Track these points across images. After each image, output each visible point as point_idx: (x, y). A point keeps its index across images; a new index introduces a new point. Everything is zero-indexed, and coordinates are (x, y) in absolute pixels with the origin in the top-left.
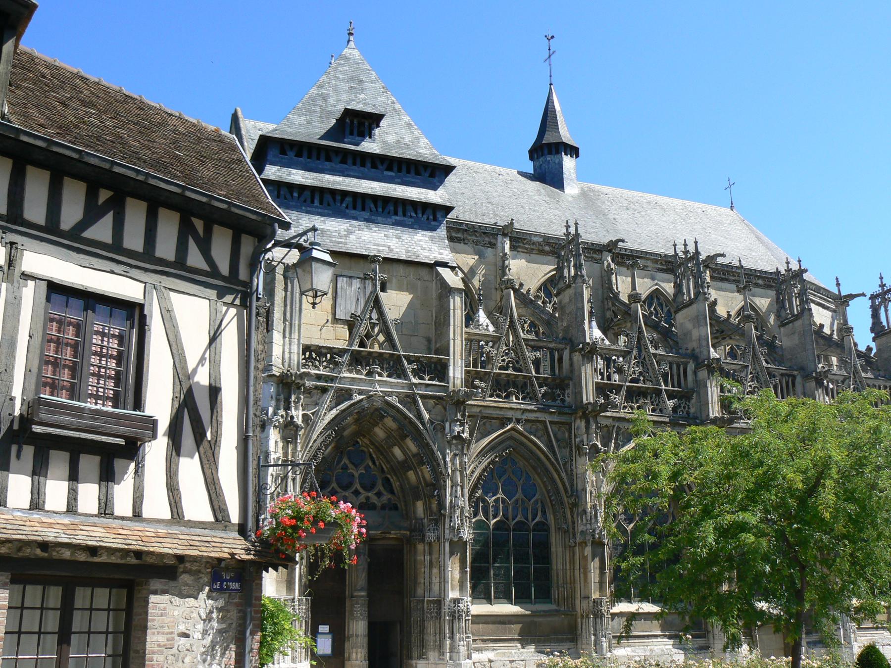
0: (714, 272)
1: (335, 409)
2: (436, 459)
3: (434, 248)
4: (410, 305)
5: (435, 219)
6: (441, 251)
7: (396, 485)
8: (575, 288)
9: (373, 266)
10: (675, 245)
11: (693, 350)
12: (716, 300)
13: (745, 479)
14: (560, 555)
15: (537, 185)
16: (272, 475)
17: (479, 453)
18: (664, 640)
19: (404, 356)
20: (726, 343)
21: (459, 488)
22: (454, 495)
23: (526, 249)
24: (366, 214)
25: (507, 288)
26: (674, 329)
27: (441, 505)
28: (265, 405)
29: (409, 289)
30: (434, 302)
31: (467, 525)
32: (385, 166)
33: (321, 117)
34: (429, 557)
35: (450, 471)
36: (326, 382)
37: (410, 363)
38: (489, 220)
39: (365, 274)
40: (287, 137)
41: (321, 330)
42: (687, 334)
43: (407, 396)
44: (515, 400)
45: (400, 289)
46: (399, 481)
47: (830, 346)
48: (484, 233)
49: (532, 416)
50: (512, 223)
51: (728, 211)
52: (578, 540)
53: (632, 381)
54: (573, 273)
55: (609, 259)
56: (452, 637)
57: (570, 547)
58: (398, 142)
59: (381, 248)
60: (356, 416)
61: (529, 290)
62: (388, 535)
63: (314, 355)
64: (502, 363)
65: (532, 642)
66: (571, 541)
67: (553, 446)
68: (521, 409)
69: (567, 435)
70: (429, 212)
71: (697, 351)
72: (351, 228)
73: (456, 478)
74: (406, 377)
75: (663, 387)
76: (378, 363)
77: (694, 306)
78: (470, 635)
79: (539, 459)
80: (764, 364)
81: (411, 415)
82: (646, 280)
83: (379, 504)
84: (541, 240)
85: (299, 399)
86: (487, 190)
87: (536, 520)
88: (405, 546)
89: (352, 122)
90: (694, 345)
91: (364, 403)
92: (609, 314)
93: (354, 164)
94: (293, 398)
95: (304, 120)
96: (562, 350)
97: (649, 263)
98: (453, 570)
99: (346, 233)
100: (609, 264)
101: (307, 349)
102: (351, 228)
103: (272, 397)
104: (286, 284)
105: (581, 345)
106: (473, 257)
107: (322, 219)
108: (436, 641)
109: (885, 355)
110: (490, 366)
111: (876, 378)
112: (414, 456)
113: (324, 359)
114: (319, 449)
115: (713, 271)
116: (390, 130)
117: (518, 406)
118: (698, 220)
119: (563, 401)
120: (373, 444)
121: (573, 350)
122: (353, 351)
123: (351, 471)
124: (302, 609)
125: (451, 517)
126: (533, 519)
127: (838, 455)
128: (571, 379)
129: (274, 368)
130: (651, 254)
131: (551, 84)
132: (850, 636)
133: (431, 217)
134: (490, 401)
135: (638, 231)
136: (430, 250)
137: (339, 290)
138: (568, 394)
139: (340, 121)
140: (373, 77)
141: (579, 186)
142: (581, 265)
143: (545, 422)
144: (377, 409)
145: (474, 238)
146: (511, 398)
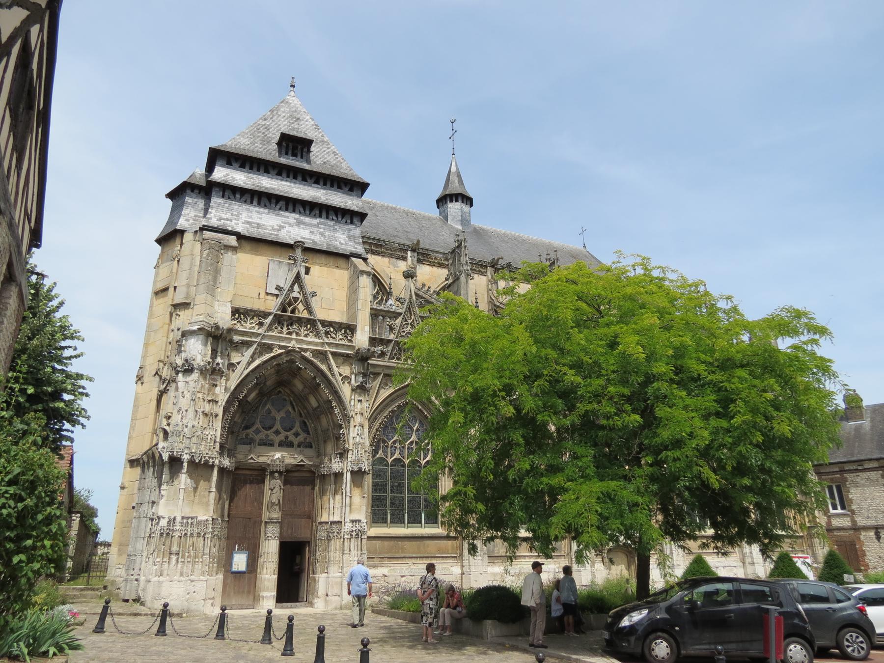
23: (430, 262)
50: (418, 241)
63: (242, 316)
126: (424, 459)
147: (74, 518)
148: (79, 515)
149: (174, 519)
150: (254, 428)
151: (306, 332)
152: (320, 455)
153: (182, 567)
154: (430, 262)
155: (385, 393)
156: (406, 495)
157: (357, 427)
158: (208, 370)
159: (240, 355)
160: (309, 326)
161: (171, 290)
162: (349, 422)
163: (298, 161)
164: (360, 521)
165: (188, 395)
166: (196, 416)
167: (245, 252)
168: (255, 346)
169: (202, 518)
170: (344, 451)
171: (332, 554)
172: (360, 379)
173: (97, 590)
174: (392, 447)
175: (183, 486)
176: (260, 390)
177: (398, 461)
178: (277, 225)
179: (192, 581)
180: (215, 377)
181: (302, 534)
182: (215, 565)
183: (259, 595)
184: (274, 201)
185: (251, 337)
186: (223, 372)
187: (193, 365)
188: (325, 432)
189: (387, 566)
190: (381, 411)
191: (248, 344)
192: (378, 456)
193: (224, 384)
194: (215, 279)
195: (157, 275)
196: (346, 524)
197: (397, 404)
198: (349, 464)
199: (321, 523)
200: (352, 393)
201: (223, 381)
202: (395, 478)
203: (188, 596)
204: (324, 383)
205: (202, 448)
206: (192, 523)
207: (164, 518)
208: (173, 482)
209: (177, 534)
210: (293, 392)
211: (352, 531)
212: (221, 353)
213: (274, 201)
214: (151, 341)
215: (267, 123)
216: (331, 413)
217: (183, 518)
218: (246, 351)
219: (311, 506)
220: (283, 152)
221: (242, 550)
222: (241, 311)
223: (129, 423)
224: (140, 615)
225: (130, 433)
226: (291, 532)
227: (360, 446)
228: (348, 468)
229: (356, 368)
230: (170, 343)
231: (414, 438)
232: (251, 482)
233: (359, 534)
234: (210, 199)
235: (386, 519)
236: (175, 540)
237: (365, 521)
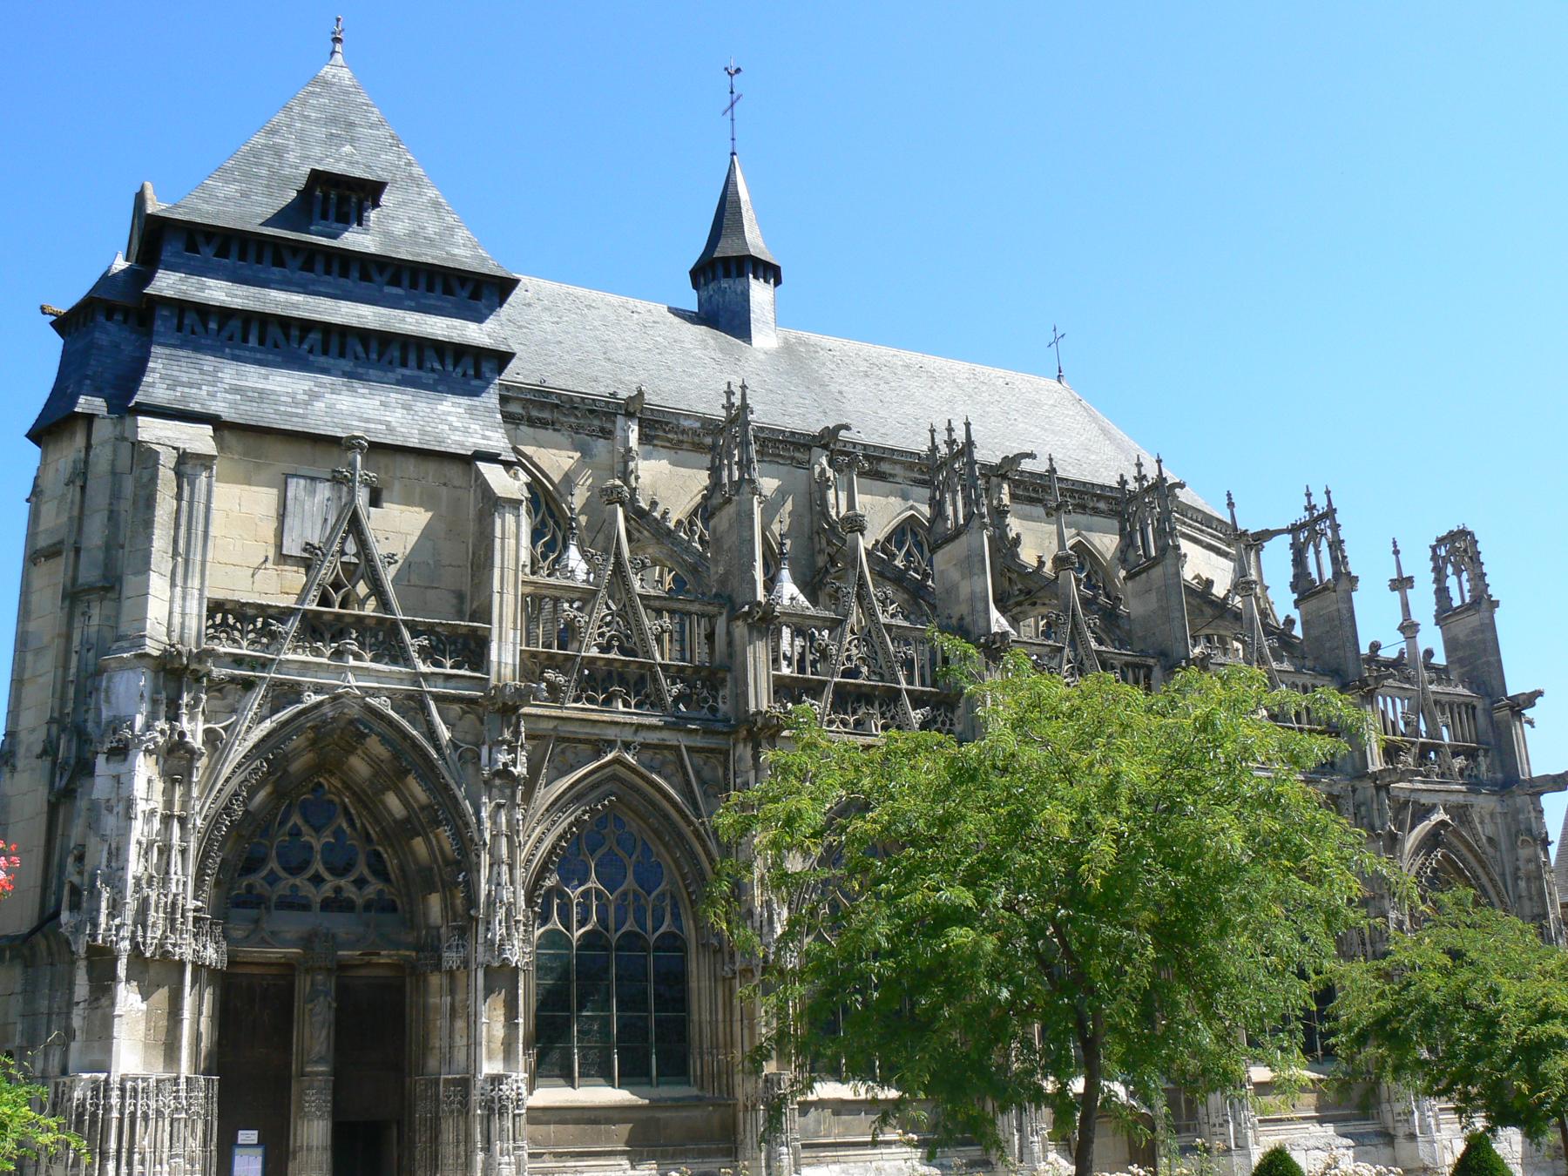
0: (1017, 487)
1: (268, 721)
2: (462, 815)
3: (474, 427)
4: (427, 533)
5: (478, 375)
6: (487, 433)
7: (392, 864)
8: (739, 503)
9: (350, 455)
10: (932, 431)
11: (961, 618)
12: (1018, 535)
13: (974, 825)
14: (705, 993)
15: (702, 330)
16: (139, 843)
17: (553, 804)
18: (904, 1150)
19: (405, 623)
20: (1035, 613)
21: (505, 868)
22: (495, 881)
23: (670, 441)
24: (346, 364)
25: (611, 503)
26: (930, 583)
27: (471, 900)
28: (130, 712)
29: (425, 503)
30: (472, 527)
31: (517, 937)
32: (386, 277)
33: (268, 186)
34: (449, 998)
35: (487, 837)
36: (253, 669)
37: (415, 634)
38: (603, 389)
39: (334, 471)
40: (198, 220)
41: (253, 575)
42: (951, 590)
43: (410, 696)
44: (621, 708)
45: (407, 501)
46: (398, 857)
47: (1221, 617)
48: (592, 411)
49: (653, 738)
51: (1055, 383)
52: (738, 966)
53: (845, 674)
54: (736, 476)
55: (824, 461)
56: (487, 1149)
57: (724, 979)
58: (413, 234)
59: (373, 426)
60: (311, 735)
61: (666, 513)
62: (375, 959)
63: (231, 621)
64: (600, 640)
65: (651, 1157)
66: (726, 968)
67: (692, 792)
68: (632, 724)
69: (720, 772)
70: (468, 362)
71: (968, 620)
72: (316, 389)
73: (500, 849)
74: (407, 661)
75: (904, 685)
76: (354, 636)
77: (964, 539)
78: (524, 1144)
79: (666, 816)
80: (1094, 645)
81: (415, 733)
82: (892, 499)
83: (360, 901)
84: (698, 425)
85: (197, 700)
86: (606, 337)
87: (662, 930)
88: (408, 980)
89: (326, 197)
90: (963, 609)
91: (326, 709)
92: (821, 560)
93: (328, 272)
94: (186, 698)
95: (237, 191)
96: (714, 616)
97: (898, 470)
98: (491, 1021)
99: (306, 397)
100: (823, 471)
101: (215, 607)
102: (316, 389)
103: (142, 696)
104: (180, 487)
105: (747, 607)
106: (571, 454)
107: (263, 371)
108: (458, 1157)
109: (1314, 632)
110: (576, 645)
111: (1298, 671)
112: (423, 808)
113: (251, 627)
114: (236, 794)
115: (1015, 484)
116: (400, 213)
117: (627, 719)
118: (996, 397)
119: (713, 710)
120: (348, 787)
121: (732, 618)
122: (306, 612)
123: (305, 838)
124: (197, 1098)
125: (488, 923)
126: (655, 929)
127: (1134, 772)
128: (729, 670)
129: (148, 641)
130: (902, 453)
131: (733, 154)
132: (1246, 1134)
133: (471, 372)
134: (573, 709)
135: (882, 413)
136: (466, 431)
137: (290, 502)
138: (724, 697)
139: (305, 194)
140: (374, 119)
141: (781, 335)
142: (750, 461)
144: (352, 722)
145: (573, 420)
146: (614, 704)
178: (305, 392)
208: (97, 999)
214: (27, 676)
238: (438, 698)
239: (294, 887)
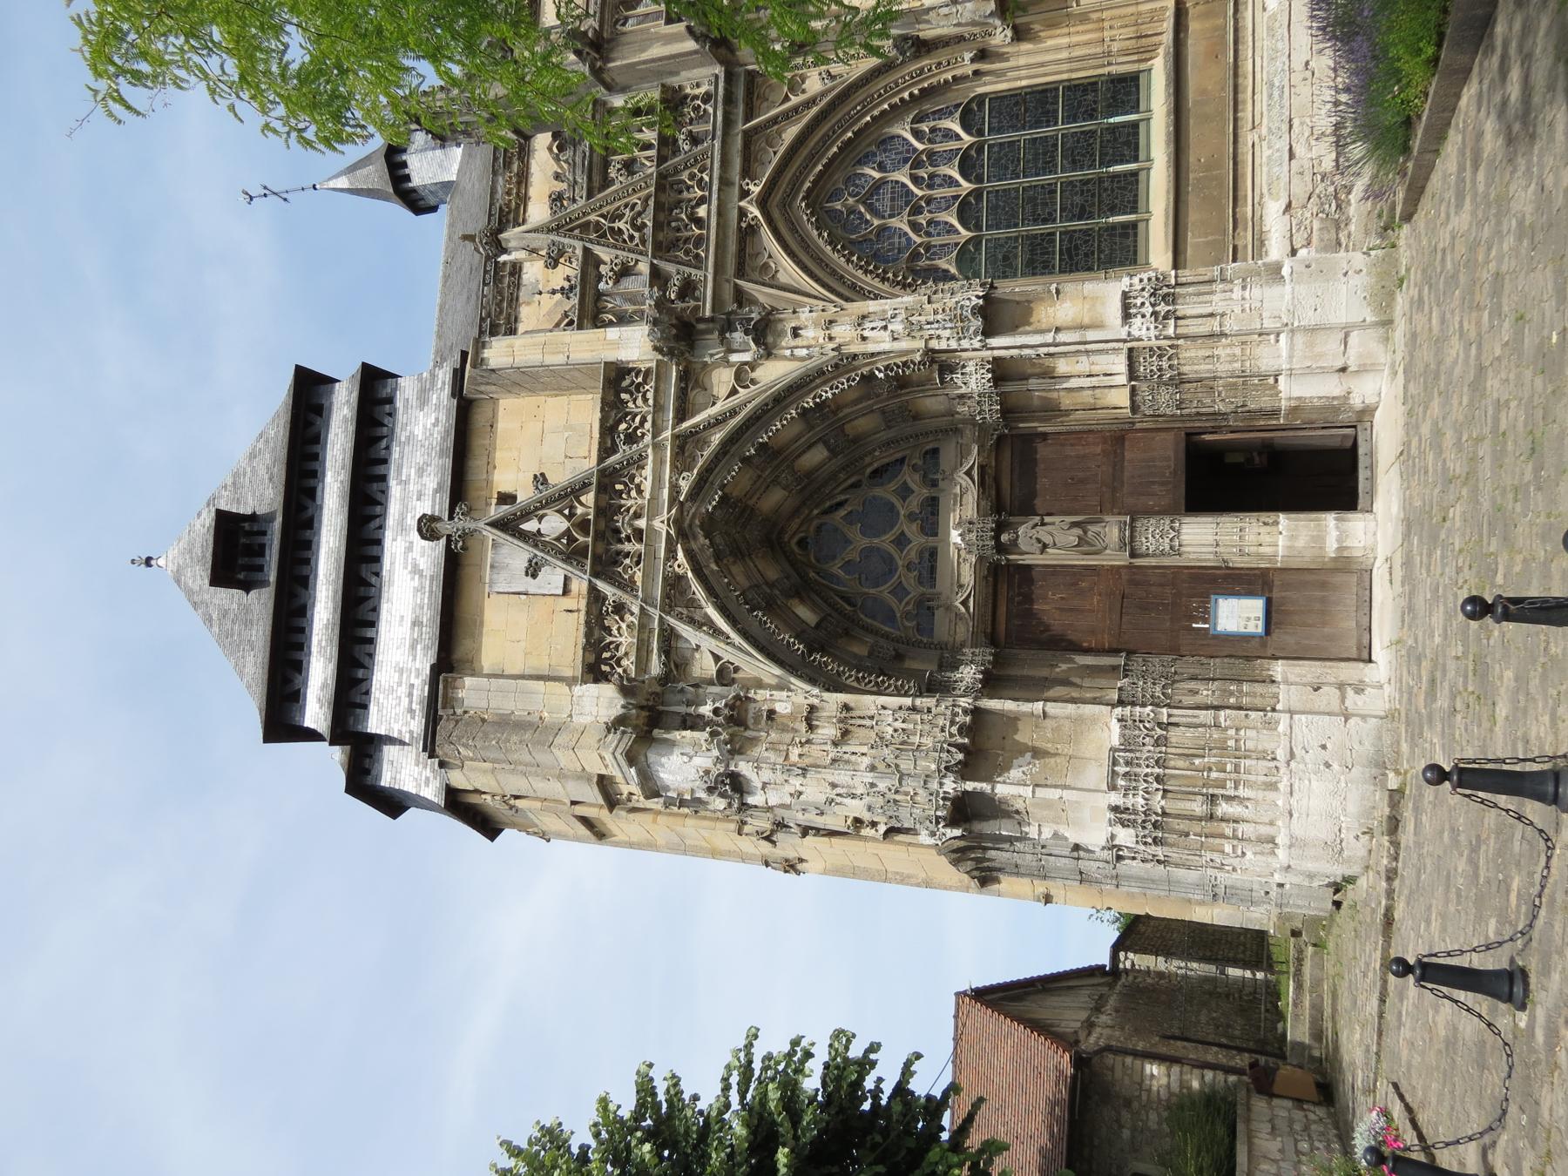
23: (518, 206)
37: (613, 450)
63: (606, 655)
126: (958, 138)
143: (745, 132)
147: (1128, 964)
148: (1122, 955)
149: (1115, 809)
150: (892, 601)
151: (633, 493)
152: (952, 428)
153: (1247, 784)
154: (518, 206)
155: (788, 270)
156: (1060, 176)
157: (866, 333)
158: (732, 736)
159: (697, 655)
160: (619, 487)
161: (580, 810)
162: (855, 356)
163: (272, 540)
164: (1125, 295)
165: (796, 783)
166: (848, 762)
167: (479, 650)
168: (672, 621)
169: (1114, 734)
170: (933, 361)
171: (1222, 368)
172: (738, 336)
173: (1300, 951)
174: (928, 234)
175: (1027, 792)
176: (789, 596)
177: (966, 211)
178: (413, 579)
179: (1292, 755)
180: (751, 715)
181: (1167, 453)
182: (1245, 687)
183: (1335, 559)
184: (362, 591)
185: (651, 631)
186: (737, 697)
187: (718, 775)
188: (889, 418)
189: (1258, 205)
190: (833, 273)
191: (669, 638)
192: (953, 270)
193: (767, 693)
194: (520, 726)
195: (561, 836)
196: (1136, 333)
197: (815, 233)
198: (965, 344)
199: (1134, 407)
200: (777, 357)
201: (761, 695)
202: (1015, 216)
203: (1335, 766)
204: (756, 434)
205: (928, 742)
206: (1127, 763)
207: (1113, 837)
208: (1017, 812)
209: (1158, 802)
210: (795, 512)
211: (1155, 314)
212: (689, 704)
213: (362, 591)
215: (215, 617)
216: (839, 408)
217: (1113, 787)
218: (687, 641)
219: (1091, 438)
220: (259, 576)
221: (1207, 611)
222: (591, 658)
223: (893, 886)
224: (1389, 911)
225: (918, 885)
226: (1163, 484)
227: (914, 319)
228: (977, 345)
229: (712, 352)
230: (696, 812)
231: (902, 176)
232: (1028, 599)
233: (1164, 293)
234: (379, 737)
235: (1124, 225)
236: (1174, 806)
237: (1126, 280)
238: (681, 415)
239: (909, 567)
